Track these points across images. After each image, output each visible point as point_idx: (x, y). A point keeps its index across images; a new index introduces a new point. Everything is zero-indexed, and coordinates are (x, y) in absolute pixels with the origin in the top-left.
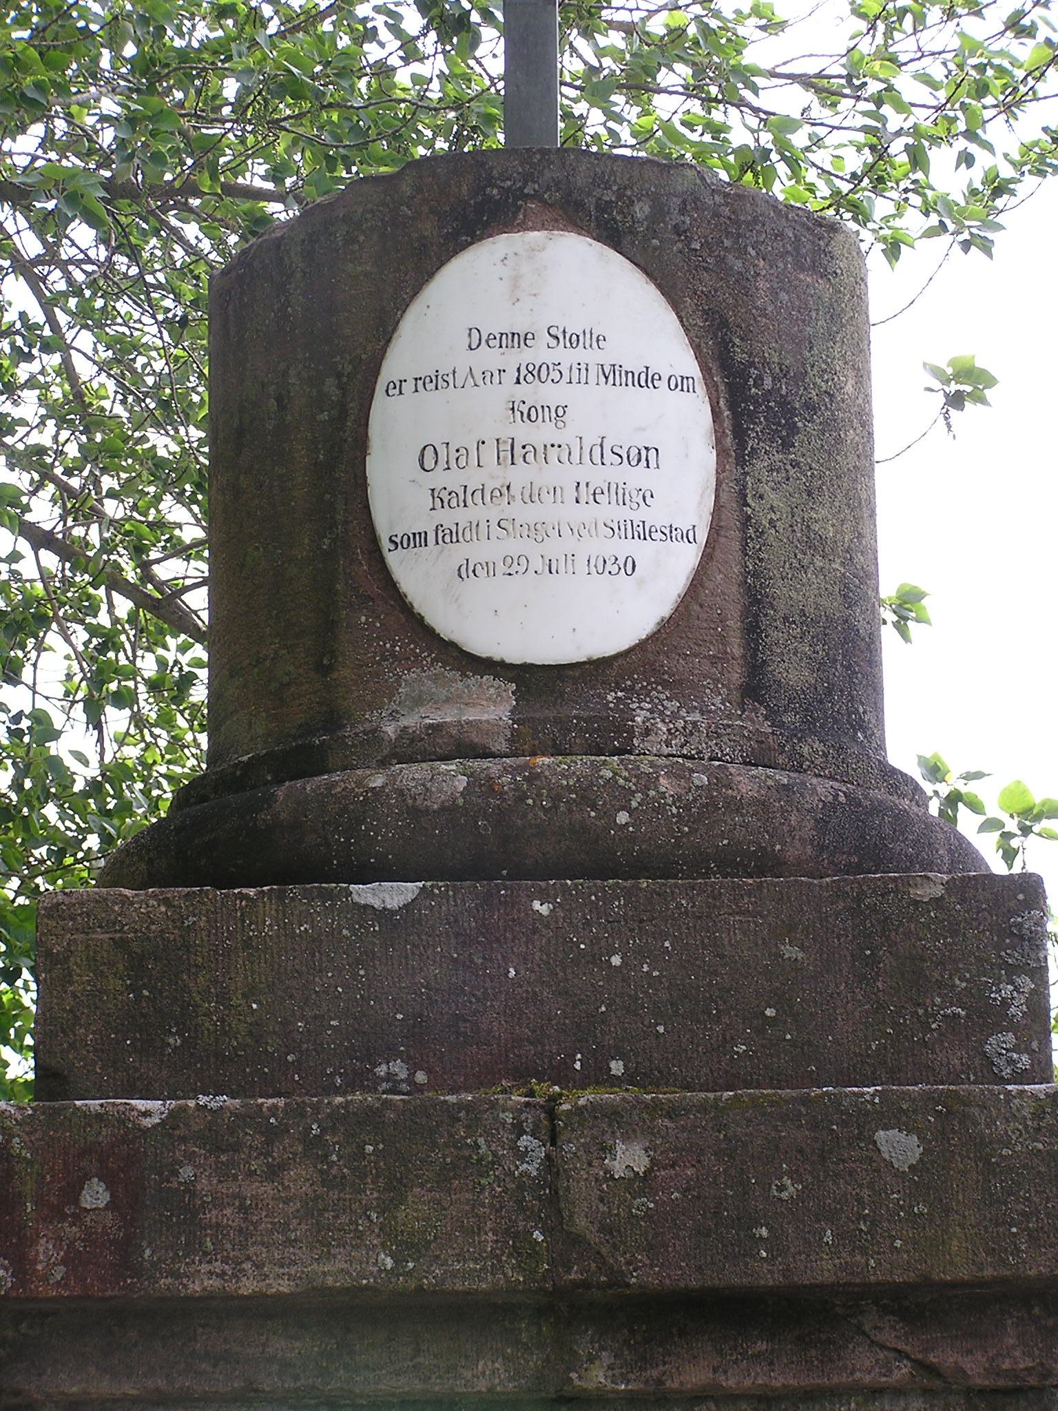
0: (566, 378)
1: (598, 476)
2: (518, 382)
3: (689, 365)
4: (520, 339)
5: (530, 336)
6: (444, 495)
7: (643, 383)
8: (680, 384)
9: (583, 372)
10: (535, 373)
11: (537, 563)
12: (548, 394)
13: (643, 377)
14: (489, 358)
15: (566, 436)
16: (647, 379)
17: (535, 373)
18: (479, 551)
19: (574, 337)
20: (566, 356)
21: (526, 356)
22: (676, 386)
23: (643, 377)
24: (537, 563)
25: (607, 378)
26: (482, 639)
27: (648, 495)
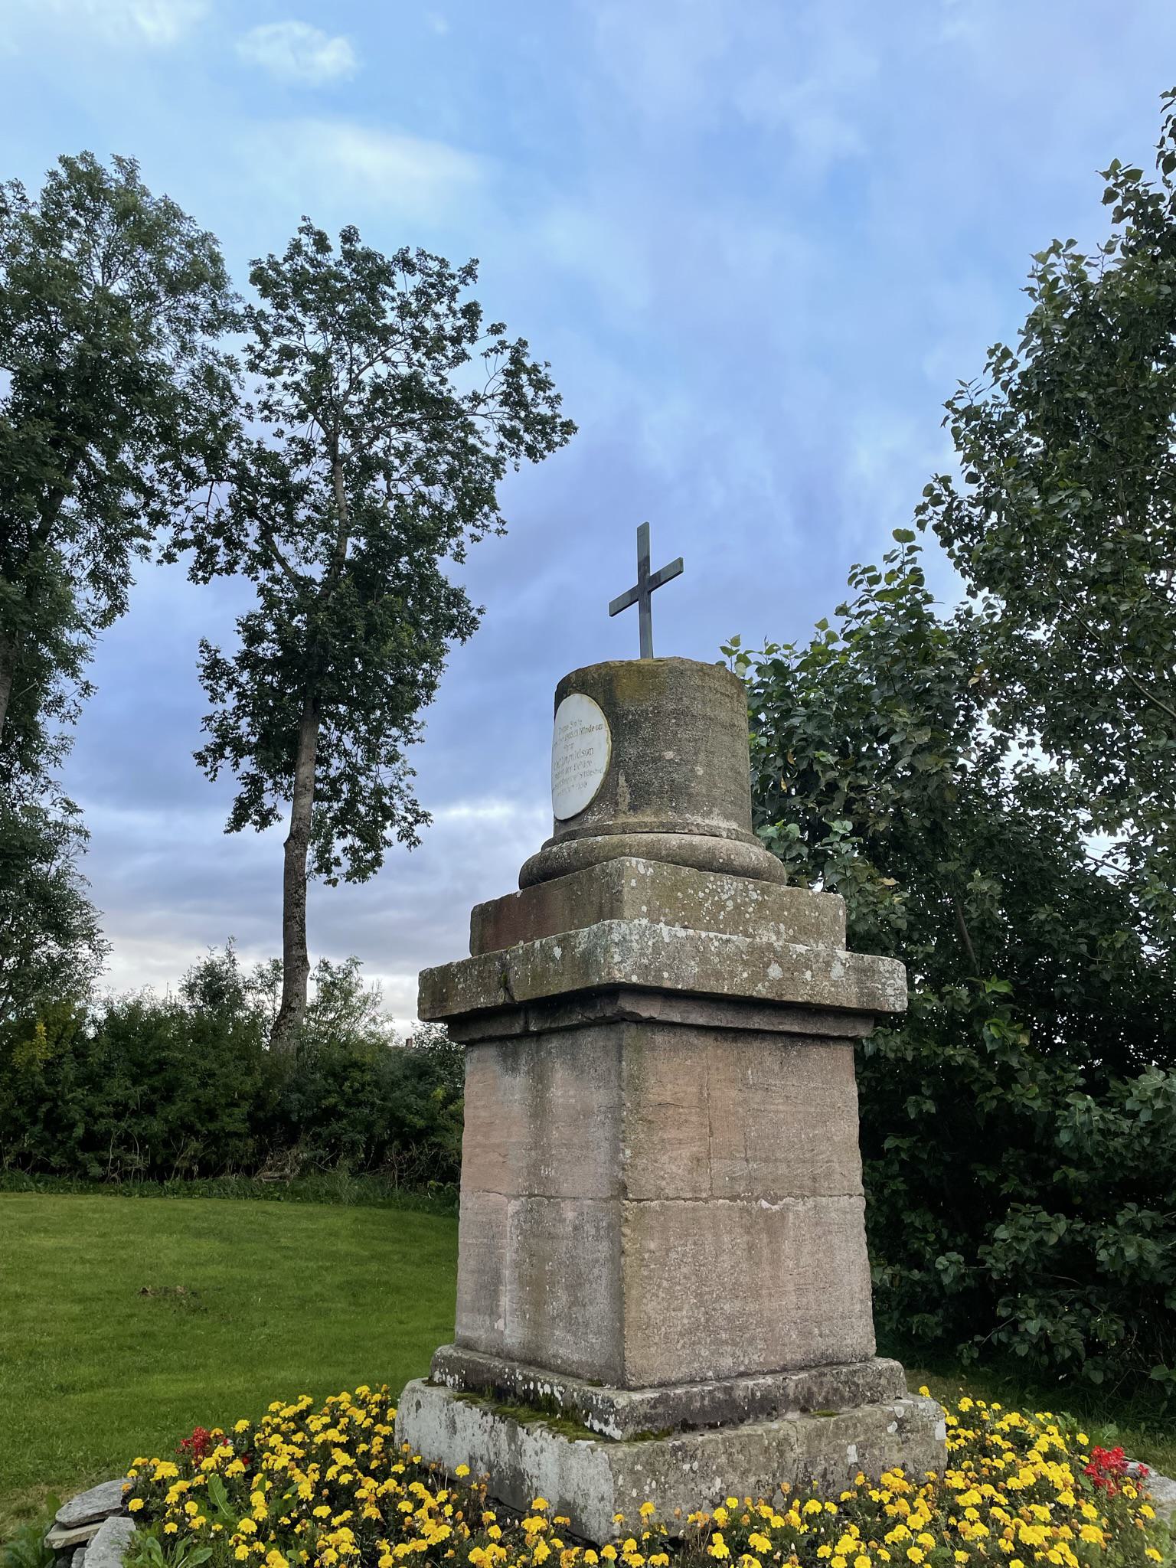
16: (591, 729)
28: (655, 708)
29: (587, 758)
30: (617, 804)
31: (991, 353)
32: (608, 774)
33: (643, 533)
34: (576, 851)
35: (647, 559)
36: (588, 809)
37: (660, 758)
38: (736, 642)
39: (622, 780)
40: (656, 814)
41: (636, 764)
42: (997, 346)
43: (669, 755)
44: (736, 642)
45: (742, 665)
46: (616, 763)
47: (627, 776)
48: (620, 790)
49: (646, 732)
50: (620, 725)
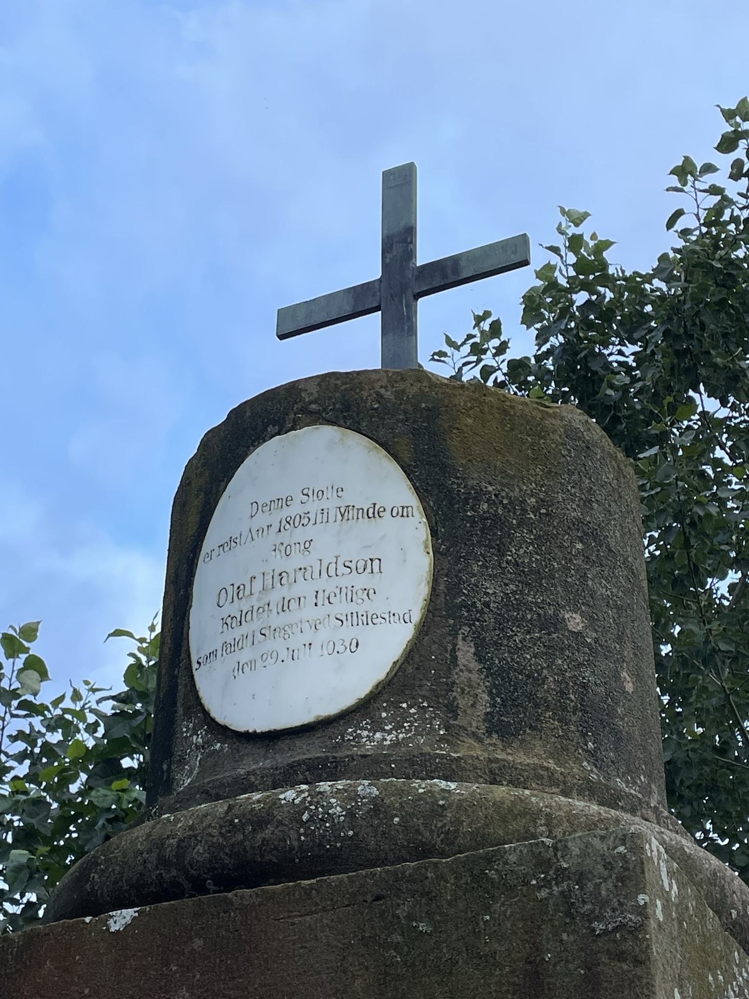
0: (312, 521)
1: (328, 585)
2: (280, 531)
3: (411, 499)
4: (287, 501)
5: (289, 498)
6: (229, 621)
7: (371, 515)
8: (403, 512)
9: (325, 514)
10: (291, 522)
11: (284, 655)
12: (300, 534)
13: (371, 511)
14: (262, 520)
15: (311, 560)
16: (374, 513)
17: (291, 522)
18: (245, 656)
19: (320, 493)
20: (313, 507)
21: (286, 512)
22: (398, 514)
23: (371, 511)
24: (284, 655)
25: (342, 516)
26: (220, 714)
27: (371, 592)
28: (542, 502)
29: (361, 581)
30: (452, 710)
31: (479, 319)
32: (424, 629)
33: (400, 185)
34: (377, 807)
35: (409, 233)
36: (363, 710)
37: (554, 624)
38: (30, 632)
39: (466, 653)
40: (557, 755)
41: (501, 623)
42: (487, 314)
43: (575, 622)
44: (30, 632)
45: (33, 675)
46: (446, 607)
47: (481, 646)
48: (461, 678)
49: (522, 550)
50: (458, 526)
